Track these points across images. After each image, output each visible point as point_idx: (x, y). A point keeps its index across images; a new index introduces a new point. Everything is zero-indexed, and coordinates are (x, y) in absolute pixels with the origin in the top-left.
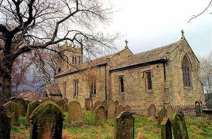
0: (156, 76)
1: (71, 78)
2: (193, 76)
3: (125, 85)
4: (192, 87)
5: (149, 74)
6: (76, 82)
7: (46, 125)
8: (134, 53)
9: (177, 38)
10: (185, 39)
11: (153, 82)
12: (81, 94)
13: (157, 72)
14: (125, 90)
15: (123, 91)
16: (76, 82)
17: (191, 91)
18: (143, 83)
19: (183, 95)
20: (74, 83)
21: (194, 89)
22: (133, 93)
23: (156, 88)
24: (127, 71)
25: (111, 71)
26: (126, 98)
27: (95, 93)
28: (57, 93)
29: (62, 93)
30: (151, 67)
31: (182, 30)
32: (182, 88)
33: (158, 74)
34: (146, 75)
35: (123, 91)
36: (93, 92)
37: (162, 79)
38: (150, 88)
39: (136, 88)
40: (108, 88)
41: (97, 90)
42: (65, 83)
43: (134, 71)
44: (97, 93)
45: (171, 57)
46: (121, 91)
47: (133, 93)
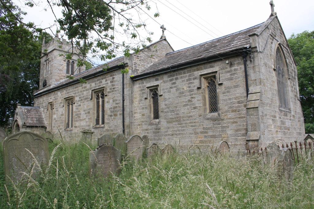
0: (226, 83)
1: (61, 95)
2: (290, 89)
3: (162, 105)
4: (290, 109)
5: (211, 79)
6: (70, 101)
7: (252, 118)
8: (176, 49)
9: (263, 17)
10: (276, 17)
11: (221, 97)
12: (77, 124)
13: (228, 75)
14: (160, 114)
15: (156, 116)
16: (70, 101)
17: (289, 115)
18: (201, 100)
19: (279, 124)
20: (66, 106)
21: (293, 113)
22: (178, 120)
23: (226, 108)
24: (166, 78)
25: (134, 79)
26: (163, 130)
27: (103, 123)
28: (34, 122)
29: (46, 123)
30: (216, 67)
31: (272, 1)
32: (277, 110)
33: (231, 79)
34: (205, 84)
35: (156, 116)
36: (100, 120)
37: (241, 90)
38: (214, 107)
39: (183, 111)
40: (127, 110)
41: (106, 117)
42: (51, 104)
43: (179, 76)
44: (106, 121)
45: (259, 43)
46: (152, 116)
47: (178, 120)
